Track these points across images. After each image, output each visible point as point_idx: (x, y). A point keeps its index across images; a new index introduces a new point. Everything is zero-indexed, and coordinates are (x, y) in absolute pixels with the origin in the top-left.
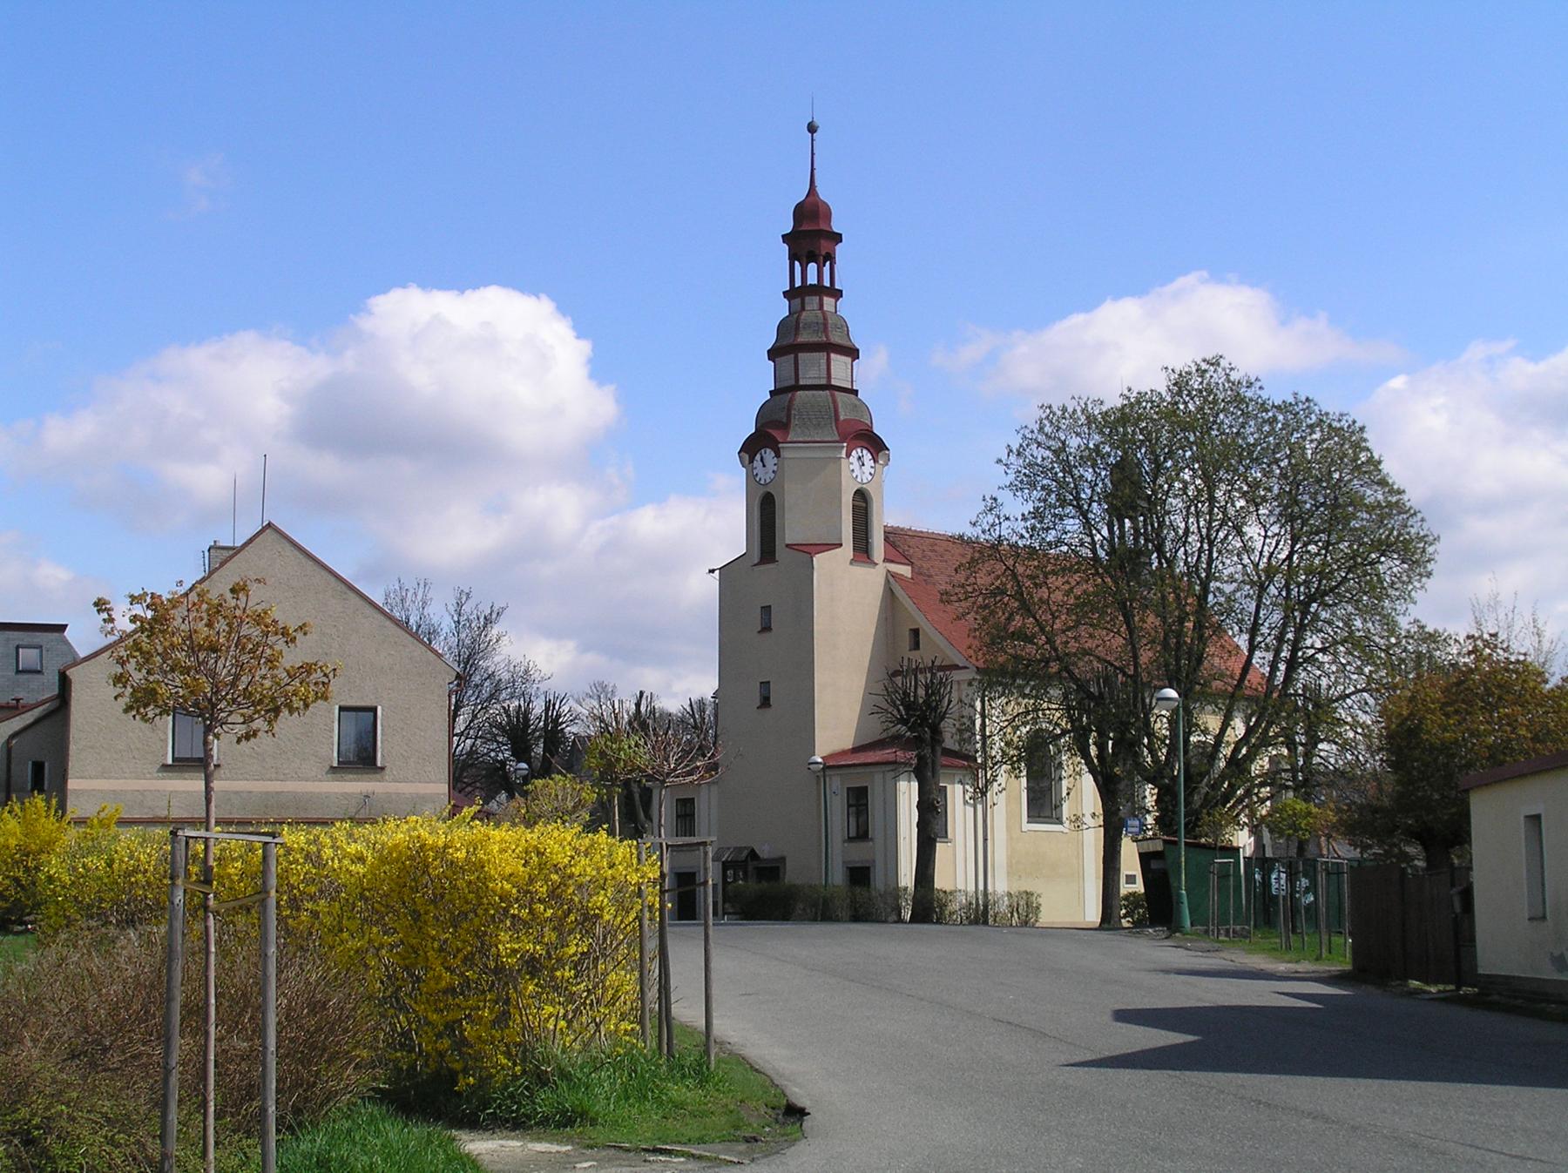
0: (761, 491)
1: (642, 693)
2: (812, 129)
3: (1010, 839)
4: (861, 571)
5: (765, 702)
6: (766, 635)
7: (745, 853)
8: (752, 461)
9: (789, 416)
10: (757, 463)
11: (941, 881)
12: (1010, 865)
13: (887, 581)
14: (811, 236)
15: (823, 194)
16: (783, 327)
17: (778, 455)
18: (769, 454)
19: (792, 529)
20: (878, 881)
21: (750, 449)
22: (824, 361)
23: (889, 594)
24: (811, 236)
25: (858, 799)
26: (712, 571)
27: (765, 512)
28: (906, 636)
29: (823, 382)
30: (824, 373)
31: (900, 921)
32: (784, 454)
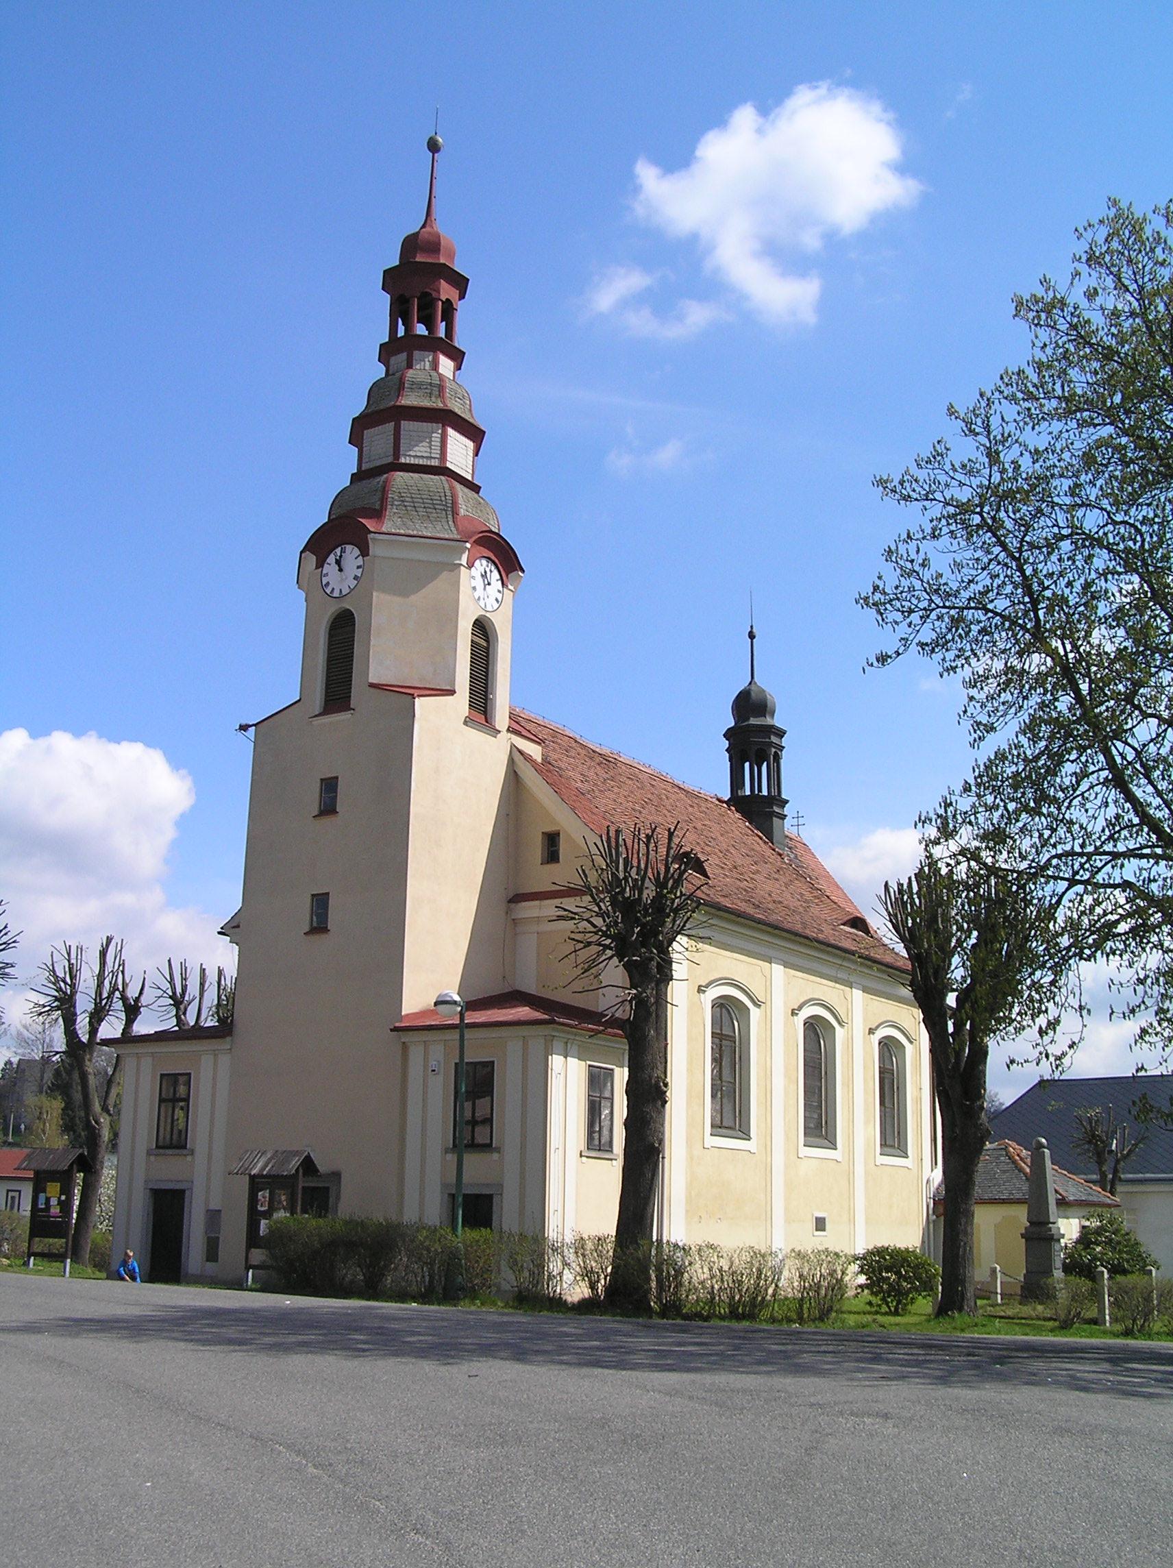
0: (332, 609)
1: (109, 940)
2: (433, 147)
3: (690, 1157)
4: (475, 736)
5: (319, 927)
6: (327, 821)
7: (295, 1162)
8: (320, 564)
9: (383, 499)
10: (330, 567)
11: (677, 1223)
12: (689, 1199)
13: (511, 761)
14: (421, 289)
15: (443, 227)
16: (376, 391)
17: (364, 552)
18: (351, 552)
19: (381, 661)
20: (507, 1215)
21: (321, 545)
22: (436, 436)
23: (513, 780)
24: (421, 289)
25: (476, 1083)
26: (244, 728)
27: (340, 640)
28: (537, 849)
29: (435, 463)
30: (436, 453)
31: (649, 1312)
32: (373, 549)
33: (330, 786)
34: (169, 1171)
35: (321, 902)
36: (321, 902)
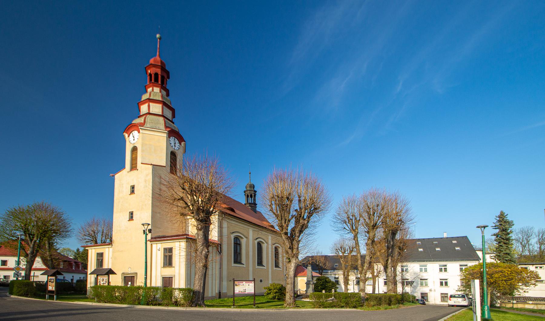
0: (132, 146)
33: (133, 187)
34: (168, 272)
35: (131, 214)
36: (131, 214)
